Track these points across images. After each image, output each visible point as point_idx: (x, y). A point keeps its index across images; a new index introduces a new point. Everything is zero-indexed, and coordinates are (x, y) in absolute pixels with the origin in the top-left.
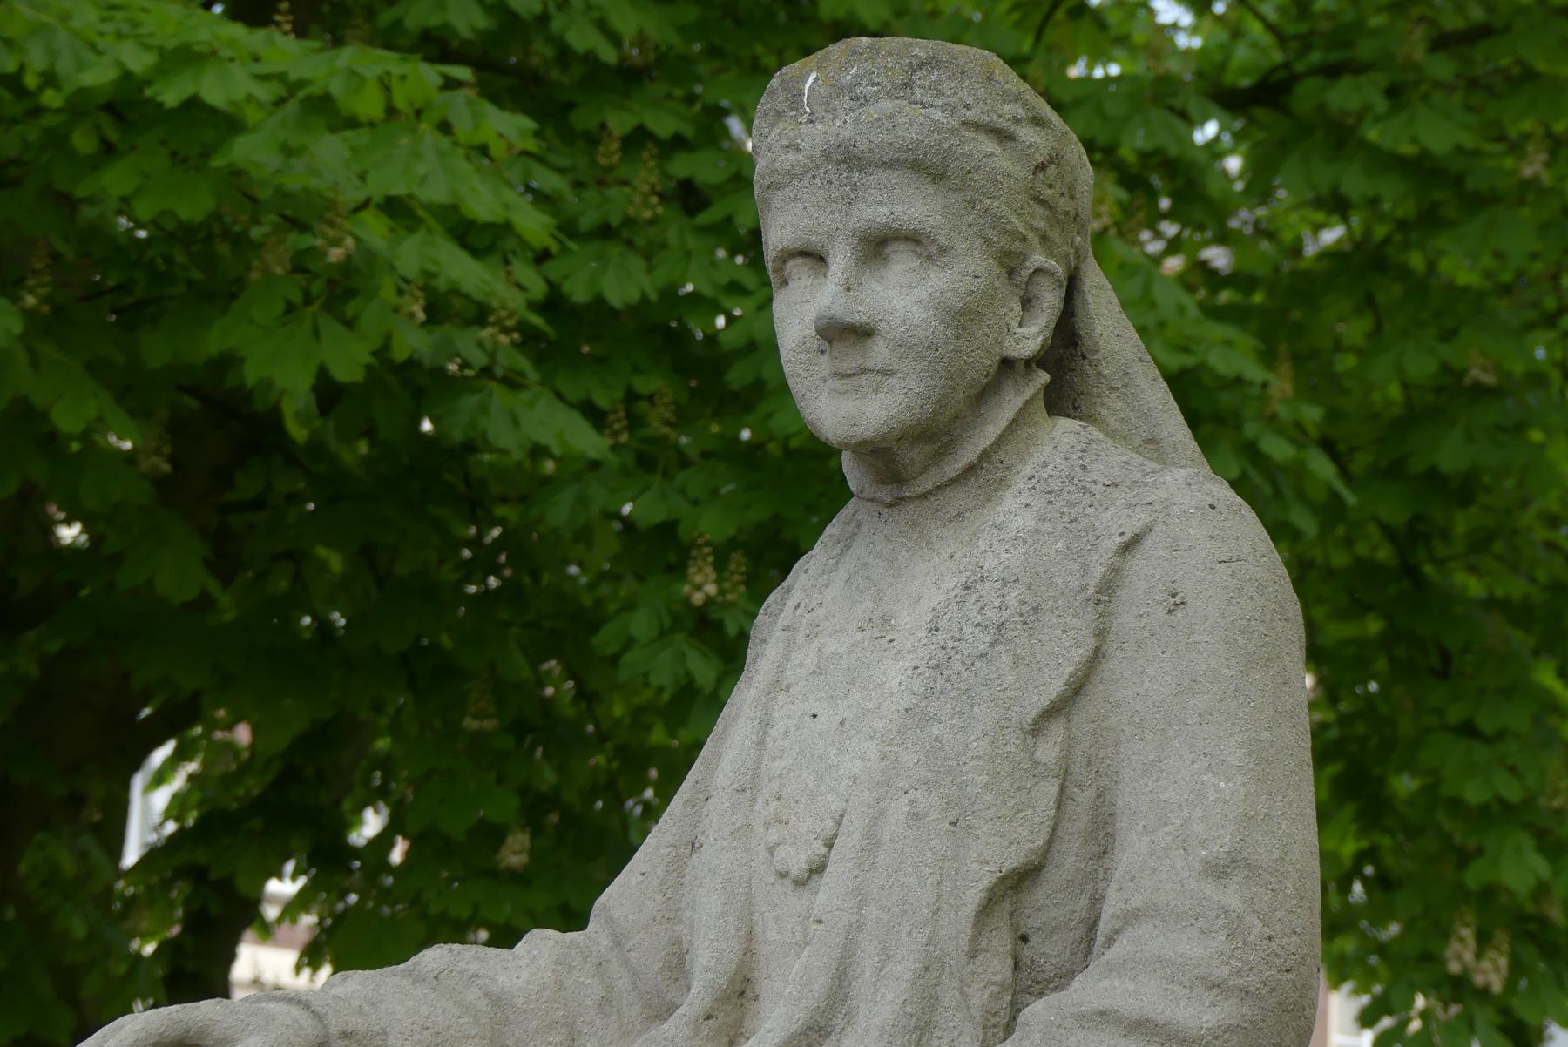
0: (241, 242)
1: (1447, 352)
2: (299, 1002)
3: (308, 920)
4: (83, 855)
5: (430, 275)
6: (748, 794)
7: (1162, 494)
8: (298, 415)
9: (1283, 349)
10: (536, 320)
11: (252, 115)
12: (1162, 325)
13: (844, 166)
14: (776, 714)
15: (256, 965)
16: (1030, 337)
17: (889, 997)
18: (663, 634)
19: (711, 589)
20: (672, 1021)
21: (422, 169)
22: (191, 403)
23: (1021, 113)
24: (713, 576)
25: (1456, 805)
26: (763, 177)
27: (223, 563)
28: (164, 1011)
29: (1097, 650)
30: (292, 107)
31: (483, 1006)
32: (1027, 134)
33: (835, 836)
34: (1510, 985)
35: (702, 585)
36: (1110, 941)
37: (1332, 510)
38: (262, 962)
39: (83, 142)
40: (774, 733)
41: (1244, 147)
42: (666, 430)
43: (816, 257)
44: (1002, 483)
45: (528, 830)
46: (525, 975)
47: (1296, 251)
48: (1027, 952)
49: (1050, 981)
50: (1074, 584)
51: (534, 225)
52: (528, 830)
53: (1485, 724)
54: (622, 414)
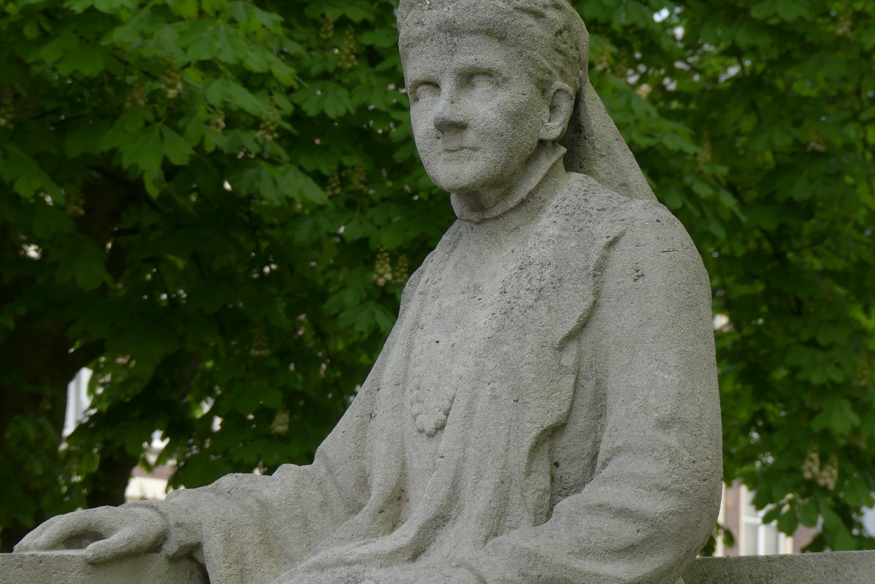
0: (122, 87)
1: (797, 133)
2: (152, 507)
3: (172, 462)
4: (41, 428)
5: (225, 103)
6: (401, 386)
7: (630, 214)
8: (154, 181)
9: (706, 134)
10: (288, 126)
11: (124, 16)
12: (637, 122)
13: (449, 34)
14: (416, 341)
15: (142, 489)
16: (555, 128)
17: (481, 499)
18: (362, 302)
19: (389, 276)
20: (361, 514)
21: (218, 45)
22: (96, 175)
24: (389, 269)
25: (807, 385)
26: (403, 40)
27: (116, 264)
29: (595, 302)
30: (146, 11)
31: (256, 507)
32: (551, 14)
33: (450, 409)
34: (839, 485)
35: (384, 274)
36: (605, 465)
37: (733, 225)
38: (146, 487)
39: (30, 32)
40: (415, 352)
41: (685, 21)
42: (361, 186)
43: (434, 85)
44: (541, 210)
45: (287, 412)
46: (278, 490)
47: (715, 80)
48: (558, 472)
49: (571, 488)
50: (582, 265)
51: (285, 73)
52: (287, 412)
53: (822, 340)
54: (337, 178)
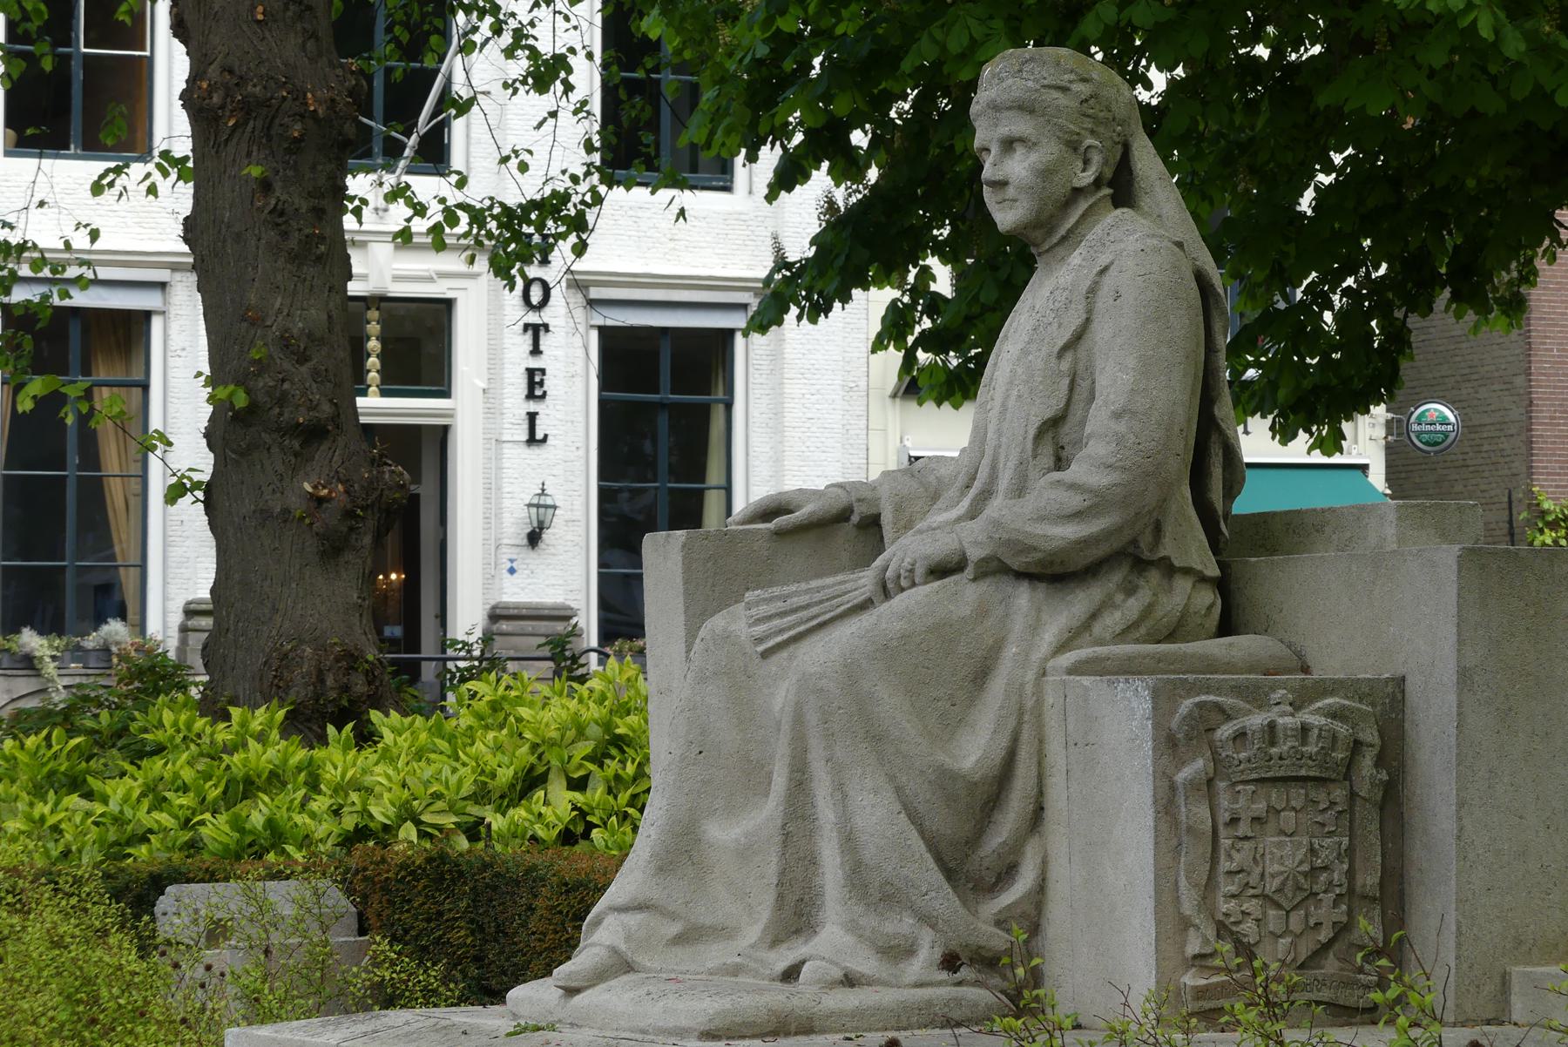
23: (1073, 77)
28: (1319, 504)
